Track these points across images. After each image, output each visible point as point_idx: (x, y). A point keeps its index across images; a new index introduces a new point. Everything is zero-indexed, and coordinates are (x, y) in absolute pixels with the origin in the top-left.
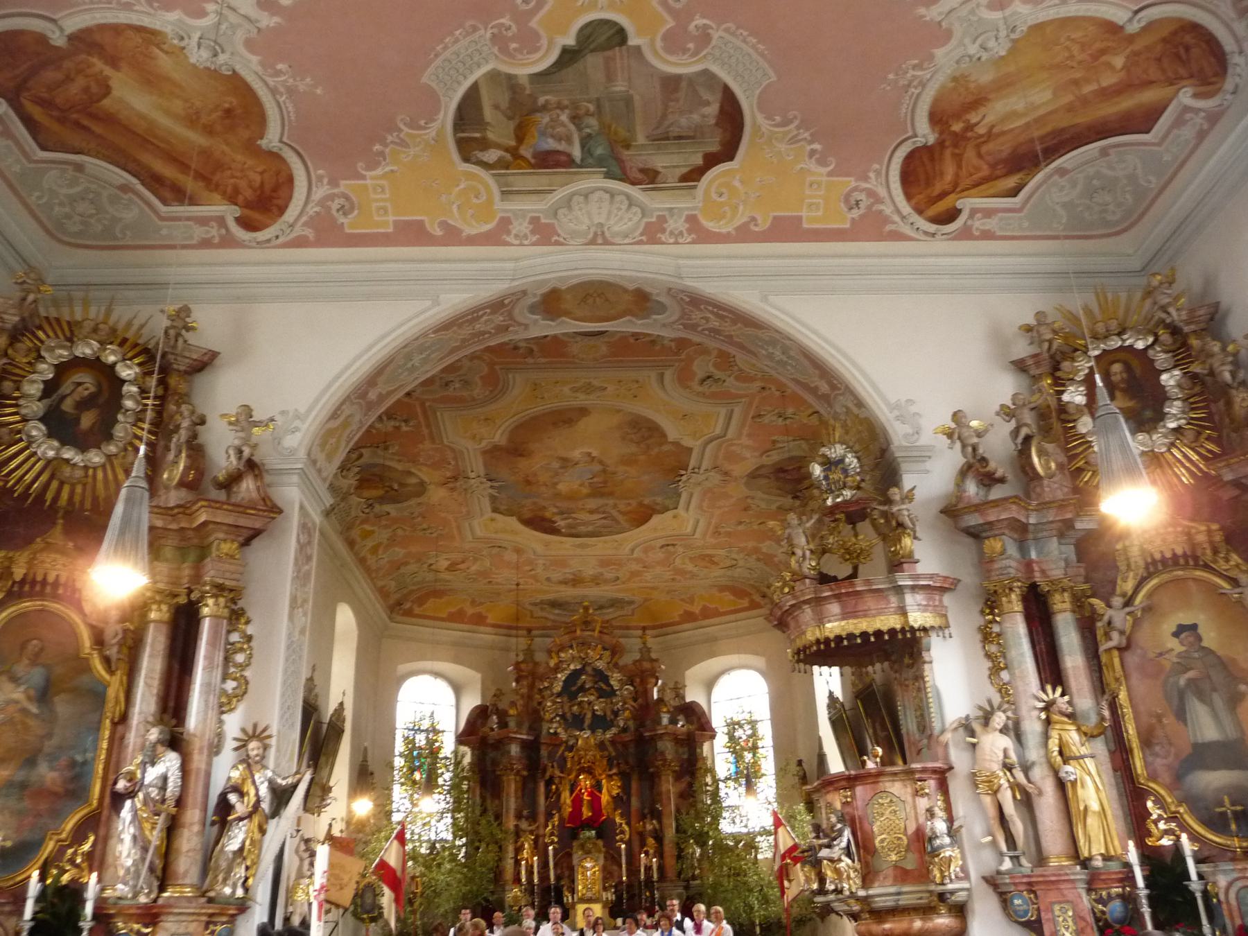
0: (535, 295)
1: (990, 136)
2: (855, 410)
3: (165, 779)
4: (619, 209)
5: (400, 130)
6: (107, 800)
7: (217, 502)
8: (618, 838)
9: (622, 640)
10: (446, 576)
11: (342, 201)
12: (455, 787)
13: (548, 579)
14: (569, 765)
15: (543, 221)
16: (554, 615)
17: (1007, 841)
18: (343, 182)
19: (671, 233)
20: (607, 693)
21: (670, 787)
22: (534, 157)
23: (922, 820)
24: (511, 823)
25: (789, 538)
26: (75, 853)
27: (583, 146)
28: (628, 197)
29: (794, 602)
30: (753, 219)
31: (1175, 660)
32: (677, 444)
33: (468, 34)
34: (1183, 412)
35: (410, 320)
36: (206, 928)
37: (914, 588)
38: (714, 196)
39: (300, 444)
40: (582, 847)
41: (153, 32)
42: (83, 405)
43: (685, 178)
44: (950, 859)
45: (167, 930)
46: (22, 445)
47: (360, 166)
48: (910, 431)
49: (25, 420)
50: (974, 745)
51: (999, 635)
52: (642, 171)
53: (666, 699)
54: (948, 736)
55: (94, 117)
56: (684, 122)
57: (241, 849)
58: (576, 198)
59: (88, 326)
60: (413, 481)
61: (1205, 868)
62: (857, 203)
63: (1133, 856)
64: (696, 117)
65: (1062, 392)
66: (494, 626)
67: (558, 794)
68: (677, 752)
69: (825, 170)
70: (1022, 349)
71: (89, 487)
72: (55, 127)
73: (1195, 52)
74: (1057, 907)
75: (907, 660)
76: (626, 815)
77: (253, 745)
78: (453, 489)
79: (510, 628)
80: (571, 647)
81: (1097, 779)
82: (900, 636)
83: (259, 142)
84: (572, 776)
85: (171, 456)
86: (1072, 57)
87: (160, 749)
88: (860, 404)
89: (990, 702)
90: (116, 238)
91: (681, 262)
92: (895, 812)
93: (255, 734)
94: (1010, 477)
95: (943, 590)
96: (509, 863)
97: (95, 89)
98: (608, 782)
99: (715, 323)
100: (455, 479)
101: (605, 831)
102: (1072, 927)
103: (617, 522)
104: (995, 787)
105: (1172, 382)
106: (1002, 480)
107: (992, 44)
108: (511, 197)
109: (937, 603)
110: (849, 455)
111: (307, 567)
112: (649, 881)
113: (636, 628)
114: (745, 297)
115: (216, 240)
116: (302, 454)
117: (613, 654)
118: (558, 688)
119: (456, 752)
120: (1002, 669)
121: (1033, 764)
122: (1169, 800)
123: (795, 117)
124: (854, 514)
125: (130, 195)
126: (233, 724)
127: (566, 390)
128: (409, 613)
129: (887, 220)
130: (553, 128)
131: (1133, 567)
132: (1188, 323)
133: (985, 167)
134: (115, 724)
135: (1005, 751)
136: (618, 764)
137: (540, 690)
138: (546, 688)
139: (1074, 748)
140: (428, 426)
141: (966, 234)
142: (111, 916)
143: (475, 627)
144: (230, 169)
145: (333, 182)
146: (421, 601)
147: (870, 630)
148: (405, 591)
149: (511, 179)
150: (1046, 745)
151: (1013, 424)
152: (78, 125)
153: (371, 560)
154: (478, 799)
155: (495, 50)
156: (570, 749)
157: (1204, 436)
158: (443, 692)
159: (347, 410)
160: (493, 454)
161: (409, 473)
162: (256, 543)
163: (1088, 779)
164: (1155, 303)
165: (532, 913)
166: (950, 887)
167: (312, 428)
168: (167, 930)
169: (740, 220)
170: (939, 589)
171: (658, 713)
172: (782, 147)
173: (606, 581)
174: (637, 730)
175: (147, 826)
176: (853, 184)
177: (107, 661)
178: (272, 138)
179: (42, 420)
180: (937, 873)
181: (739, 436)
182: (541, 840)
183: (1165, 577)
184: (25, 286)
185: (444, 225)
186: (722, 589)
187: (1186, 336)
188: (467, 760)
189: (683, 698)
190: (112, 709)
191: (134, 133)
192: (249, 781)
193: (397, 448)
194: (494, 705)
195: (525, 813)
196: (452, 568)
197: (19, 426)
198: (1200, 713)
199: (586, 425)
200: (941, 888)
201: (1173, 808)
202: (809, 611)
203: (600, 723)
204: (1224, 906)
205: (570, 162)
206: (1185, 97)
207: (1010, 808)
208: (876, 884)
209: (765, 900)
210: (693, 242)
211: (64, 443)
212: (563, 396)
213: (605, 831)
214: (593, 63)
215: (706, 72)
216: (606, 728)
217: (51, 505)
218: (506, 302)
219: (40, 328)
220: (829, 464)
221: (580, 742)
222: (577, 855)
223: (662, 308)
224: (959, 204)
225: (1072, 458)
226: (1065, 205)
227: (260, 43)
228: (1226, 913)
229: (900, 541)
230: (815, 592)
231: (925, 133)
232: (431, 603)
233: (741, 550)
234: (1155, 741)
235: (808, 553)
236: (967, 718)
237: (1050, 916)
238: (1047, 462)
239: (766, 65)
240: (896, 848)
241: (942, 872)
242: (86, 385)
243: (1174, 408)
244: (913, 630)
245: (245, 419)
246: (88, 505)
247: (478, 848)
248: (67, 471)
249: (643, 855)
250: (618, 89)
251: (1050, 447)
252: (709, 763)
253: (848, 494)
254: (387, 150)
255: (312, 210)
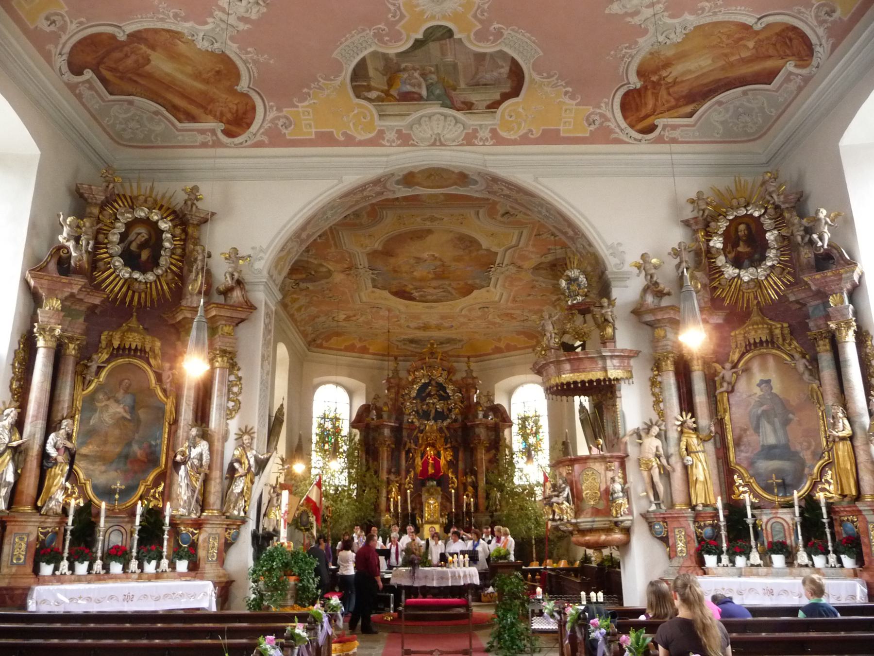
0: (399, 175)
1: (675, 83)
2: (587, 247)
3: (201, 455)
4: (449, 125)
5: (319, 81)
6: (170, 464)
7: (221, 304)
8: (450, 486)
9: (455, 364)
10: (344, 324)
11: (284, 120)
12: (349, 455)
13: (408, 327)
14: (420, 442)
15: (404, 132)
16: (412, 347)
17: (654, 495)
18: (285, 110)
19: (481, 139)
20: (445, 398)
21: (482, 456)
22: (398, 95)
23: (609, 483)
24: (384, 476)
25: (543, 326)
26: (155, 492)
27: (428, 90)
28: (455, 118)
29: (545, 362)
30: (531, 131)
31: (757, 399)
32: (488, 250)
33: (360, 33)
34: (776, 256)
35: (325, 192)
36: (226, 531)
37: (612, 357)
38: (507, 117)
39: (264, 266)
40: (428, 491)
41: (177, 33)
42: (142, 246)
43: (489, 107)
44: (621, 505)
45: (205, 531)
46: (111, 270)
47: (295, 100)
48: (619, 262)
49: (111, 256)
50: (641, 444)
51: (660, 383)
52: (464, 103)
53: (481, 402)
54: (627, 439)
55: (140, 75)
56: (488, 77)
57: (242, 492)
58: (423, 119)
59: (142, 198)
60: (324, 270)
61: (756, 512)
62: (594, 122)
63: (719, 505)
64: (495, 74)
65: (710, 240)
66: (374, 354)
67: (414, 459)
68: (488, 435)
69: (574, 102)
70: (689, 213)
71: (148, 296)
72: (118, 81)
73: (795, 42)
74: (676, 530)
75: (609, 395)
76: (456, 473)
77: (246, 437)
78: (348, 275)
79: (383, 355)
80: (423, 369)
81: (704, 464)
82: (602, 383)
83: (236, 87)
84: (422, 448)
85: (193, 276)
86: (722, 42)
87: (198, 439)
88: (590, 245)
89: (651, 421)
90: (151, 141)
91: (486, 157)
92: (595, 479)
93: (246, 431)
94: (673, 292)
95: (629, 357)
96: (383, 500)
97: (141, 61)
98: (445, 452)
99: (507, 192)
100: (350, 269)
101: (442, 482)
102: (684, 540)
103: (452, 294)
104: (650, 467)
105: (772, 238)
106: (669, 294)
107: (672, 36)
108: (385, 118)
109: (626, 364)
110: (581, 276)
111: (269, 337)
112: (468, 512)
113: (464, 356)
114: (524, 179)
115: (210, 143)
116: (265, 273)
117: (449, 373)
118: (414, 394)
119: (350, 433)
120: (661, 402)
121: (672, 455)
122: (746, 475)
123: (555, 74)
124: (584, 310)
125: (160, 116)
126: (234, 426)
127: (419, 219)
128: (320, 346)
129: (611, 131)
130: (410, 80)
131: (739, 346)
132: (784, 203)
133: (673, 100)
134: (170, 425)
135: (657, 448)
136: (451, 442)
137: (403, 395)
138: (407, 394)
139: (693, 447)
140: (334, 238)
141: (660, 140)
142: (178, 524)
143: (361, 355)
144: (218, 102)
145: (279, 109)
146: (328, 338)
147: (586, 380)
148: (318, 333)
149: (384, 107)
150: (679, 444)
151: (678, 260)
152: (130, 79)
153: (297, 316)
154: (364, 460)
155: (376, 41)
156: (421, 432)
157: (787, 271)
158: (342, 395)
159: (290, 245)
160: (373, 255)
161: (321, 265)
162: (241, 325)
163: (699, 464)
164: (766, 190)
165: (398, 529)
166: (621, 518)
167: (271, 258)
168: (205, 531)
169: (522, 131)
170: (626, 357)
171: (476, 411)
172: (548, 89)
173: (446, 328)
174: (463, 421)
175: (194, 479)
176: (592, 110)
177: (164, 391)
178: (243, 85)
179: (120, 256)
180: (614, 512)
181: (527, 245)
182: (402, 487)
183: (756, 352)
184: (107, 178)
185: (345, 134)
186: (519, 333)
187: (782, 210)
188: (357, 438)
189: (493, 401)
190: (169, 417)
191: (163, 83)
192: (245, 456)
193: (314, 251)
194: (374, 404)
195: (393, 470)
196: (348, 319)
197: (109, 260)
198: (766, 428)
199: (430, 239)
200: (615, 519)
201: (747, 480)
202: (553, 367)
203: (440, 416)
204: (764, 531)
205: (421, 98)
206: (790, 66)
207: (657, 478)
208: (582, 516)
209: (538, 524)
210: (493, 145)
211: (133, 269)
212: (417, 223)
213: (442, 482)
214: (433, 47)
215: (501, 51)
216: (443, 420)
217: (129, 305)
218: (382, 180)
219: (116, 201)
220: (570, 280)
221: (427, 427)
222: (425, 496)
223: (476, 182)
224: (656, 122)
225: (712, 280)
226: (722, 123)
227: (239, 38)
228: (765, 535)
229: (605, 329)
230: (556, 357)
231: (635, 82)
232: (334, 340)
233: (530, 311)
234: (742, 443)
235: (553, 335)
236: (638, 429)
237: (673, 534)
238: (696, 284)
239: (537, 48)
240: (593, 497)
241: (616, 511)
242: (142, 235)
243: (772, 253)
244: (610, 380)
245: (234, 256)
246: (149, 304)
247: (364, 491)
248: (136, 285)
249: (465, 497)
250: (449, 60)
251: (698, 274)
252: (507, 441)
253: (580, 298)
254: (311, 92)
255: (267, 125)
